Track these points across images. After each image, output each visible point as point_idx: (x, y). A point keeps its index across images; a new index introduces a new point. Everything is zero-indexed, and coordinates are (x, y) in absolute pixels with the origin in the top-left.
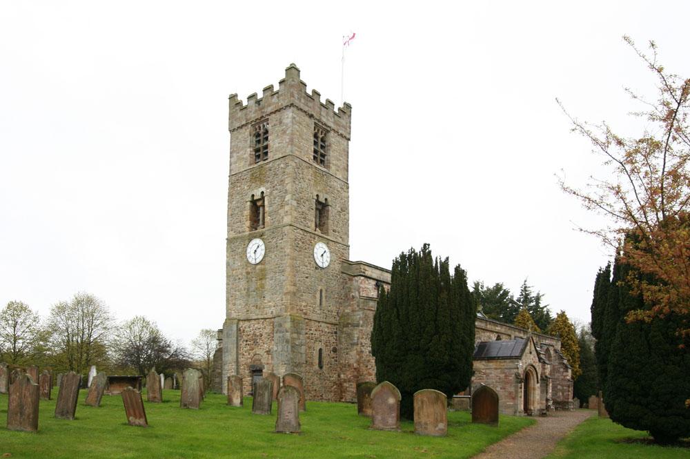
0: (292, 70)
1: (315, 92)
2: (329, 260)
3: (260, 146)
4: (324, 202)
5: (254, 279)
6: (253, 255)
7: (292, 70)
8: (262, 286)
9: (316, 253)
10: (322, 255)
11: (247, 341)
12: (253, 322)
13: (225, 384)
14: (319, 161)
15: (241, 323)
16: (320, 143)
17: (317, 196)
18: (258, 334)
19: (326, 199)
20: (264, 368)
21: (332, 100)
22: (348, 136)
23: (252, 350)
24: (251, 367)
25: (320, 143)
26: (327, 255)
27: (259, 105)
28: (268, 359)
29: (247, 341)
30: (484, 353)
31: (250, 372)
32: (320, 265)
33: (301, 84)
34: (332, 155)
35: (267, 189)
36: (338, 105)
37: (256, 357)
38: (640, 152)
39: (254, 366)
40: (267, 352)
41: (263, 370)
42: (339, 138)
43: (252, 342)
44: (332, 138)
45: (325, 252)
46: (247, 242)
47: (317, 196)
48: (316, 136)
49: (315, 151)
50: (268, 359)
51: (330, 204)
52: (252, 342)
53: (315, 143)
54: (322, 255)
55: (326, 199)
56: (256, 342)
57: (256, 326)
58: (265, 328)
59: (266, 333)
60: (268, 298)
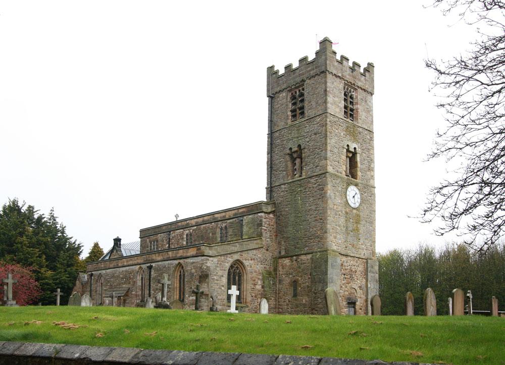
0: (325, 43)
1: (342, 57)
2: (359, 200)
3: (299, 105)
4: (354, 151)
5: (351, 220)
6: (352, 200)
7: (325, 43)
8: (358, 230)
9: (349, 195)
10: (354, 197)
12: (350, 258)
14: (349, 115)
16: (349, 100)
17: (348, 146)
18: (353, 270)
19: (355, 148)
21: (357, 61)
22: (369, 90)
23: (348, 283)
25: (349, 100)
26: (358, 197)
27: (352, 72)
32: (353, 205)
34: (360, 108)
36: (364, 65)
41: (357, 303)
42: (364, 94)
43: (349, 277)
44: (359, 95)
45: (356, 194)
47: (348, 146)
48: (345, 95)
49: (346, 107)
51: (358, 152)
52: (349, 277)
53: (345, 100)
54: (354, 197)
55: (355, 148)
56: (352, 278)
59: (360, 271)
60: (361, 241)
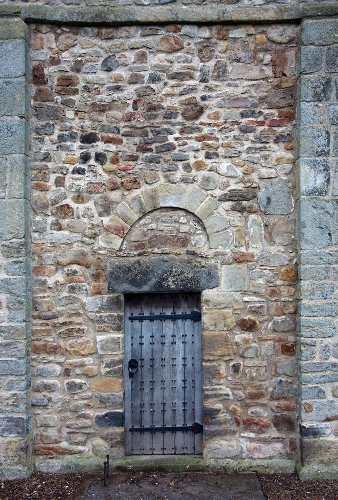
11: (89, 139)
12: (137, 37)
13: (13, 325)
15: (48, 41)
20: (213, 280)
24: (119, 274)
28: (242, 234)
29: (89, 139)
30: (309, 408)
31: (114, 304)
33: (135, 81)
35: (83, 275)
37: (163, 226)
38: (201, 371)
39: (145, 274)
40: (232, 197)
41: (207, 294)
43: (129, 146)
46: (60, 172)
50: (242, 234)
52: (129, 146)
57: (155, 60)
58: (220, 73)
59: (234, 100)
